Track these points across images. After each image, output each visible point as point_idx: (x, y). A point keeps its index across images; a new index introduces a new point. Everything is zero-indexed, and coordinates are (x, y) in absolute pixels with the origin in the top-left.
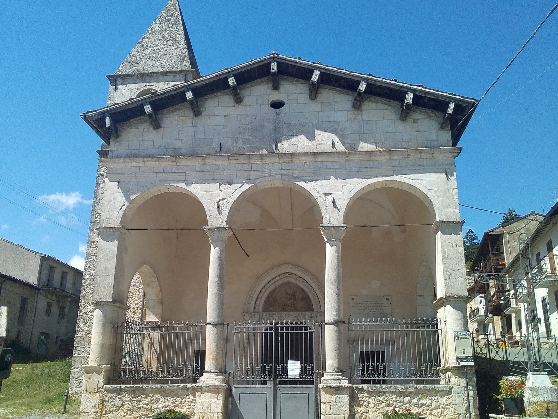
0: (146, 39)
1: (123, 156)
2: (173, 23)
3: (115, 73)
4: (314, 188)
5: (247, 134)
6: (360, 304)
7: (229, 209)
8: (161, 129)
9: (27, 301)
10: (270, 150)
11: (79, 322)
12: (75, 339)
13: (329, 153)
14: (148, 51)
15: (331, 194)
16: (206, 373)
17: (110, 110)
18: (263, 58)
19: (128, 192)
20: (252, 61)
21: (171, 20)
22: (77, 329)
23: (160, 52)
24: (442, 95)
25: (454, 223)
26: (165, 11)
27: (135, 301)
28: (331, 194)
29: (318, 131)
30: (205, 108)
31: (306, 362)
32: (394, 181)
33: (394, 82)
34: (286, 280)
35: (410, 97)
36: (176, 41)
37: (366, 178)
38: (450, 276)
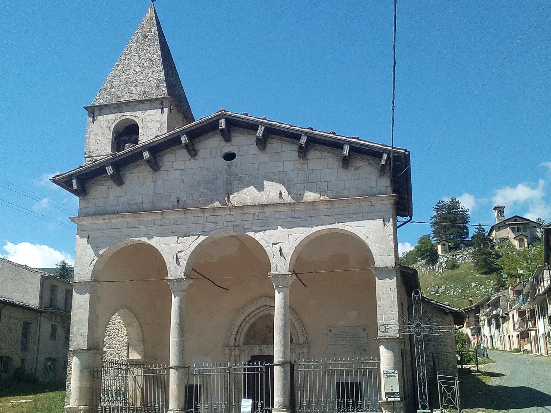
0: (123, 62)
1: (91, 213)
2: (150, 40)
3: (92, 103)
4: (263, 238)
5: (201, 187)
6: (337, 336)
7: (187, 260)
8: (124, 185)
9: (29, 326)
10: (224, 204)
11: (70, 359)
12: (67, 376)
13: (276, 205)
14: (124, 76)
15: (278, 243)
16: (170, 411)
17: (76, 173)
18: (213, 115)
19: (96, 248)
20: (202, 119)
21: (148, 37)
22: (68, 367)
23: (136, 76)
24: (376, 147)
25: (389, 268)
26: (141, 26)
27: (121, 338)
28: (278, 243)
29: (267, 181)
30: (163, 163)
31: (257, 400)
32: (336, 228)
33: (332, 135)
34: (266, 312)
35: (347, 149)
36: (153, 62)
37: (310, 227)
38: (383, 319)
